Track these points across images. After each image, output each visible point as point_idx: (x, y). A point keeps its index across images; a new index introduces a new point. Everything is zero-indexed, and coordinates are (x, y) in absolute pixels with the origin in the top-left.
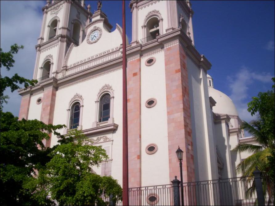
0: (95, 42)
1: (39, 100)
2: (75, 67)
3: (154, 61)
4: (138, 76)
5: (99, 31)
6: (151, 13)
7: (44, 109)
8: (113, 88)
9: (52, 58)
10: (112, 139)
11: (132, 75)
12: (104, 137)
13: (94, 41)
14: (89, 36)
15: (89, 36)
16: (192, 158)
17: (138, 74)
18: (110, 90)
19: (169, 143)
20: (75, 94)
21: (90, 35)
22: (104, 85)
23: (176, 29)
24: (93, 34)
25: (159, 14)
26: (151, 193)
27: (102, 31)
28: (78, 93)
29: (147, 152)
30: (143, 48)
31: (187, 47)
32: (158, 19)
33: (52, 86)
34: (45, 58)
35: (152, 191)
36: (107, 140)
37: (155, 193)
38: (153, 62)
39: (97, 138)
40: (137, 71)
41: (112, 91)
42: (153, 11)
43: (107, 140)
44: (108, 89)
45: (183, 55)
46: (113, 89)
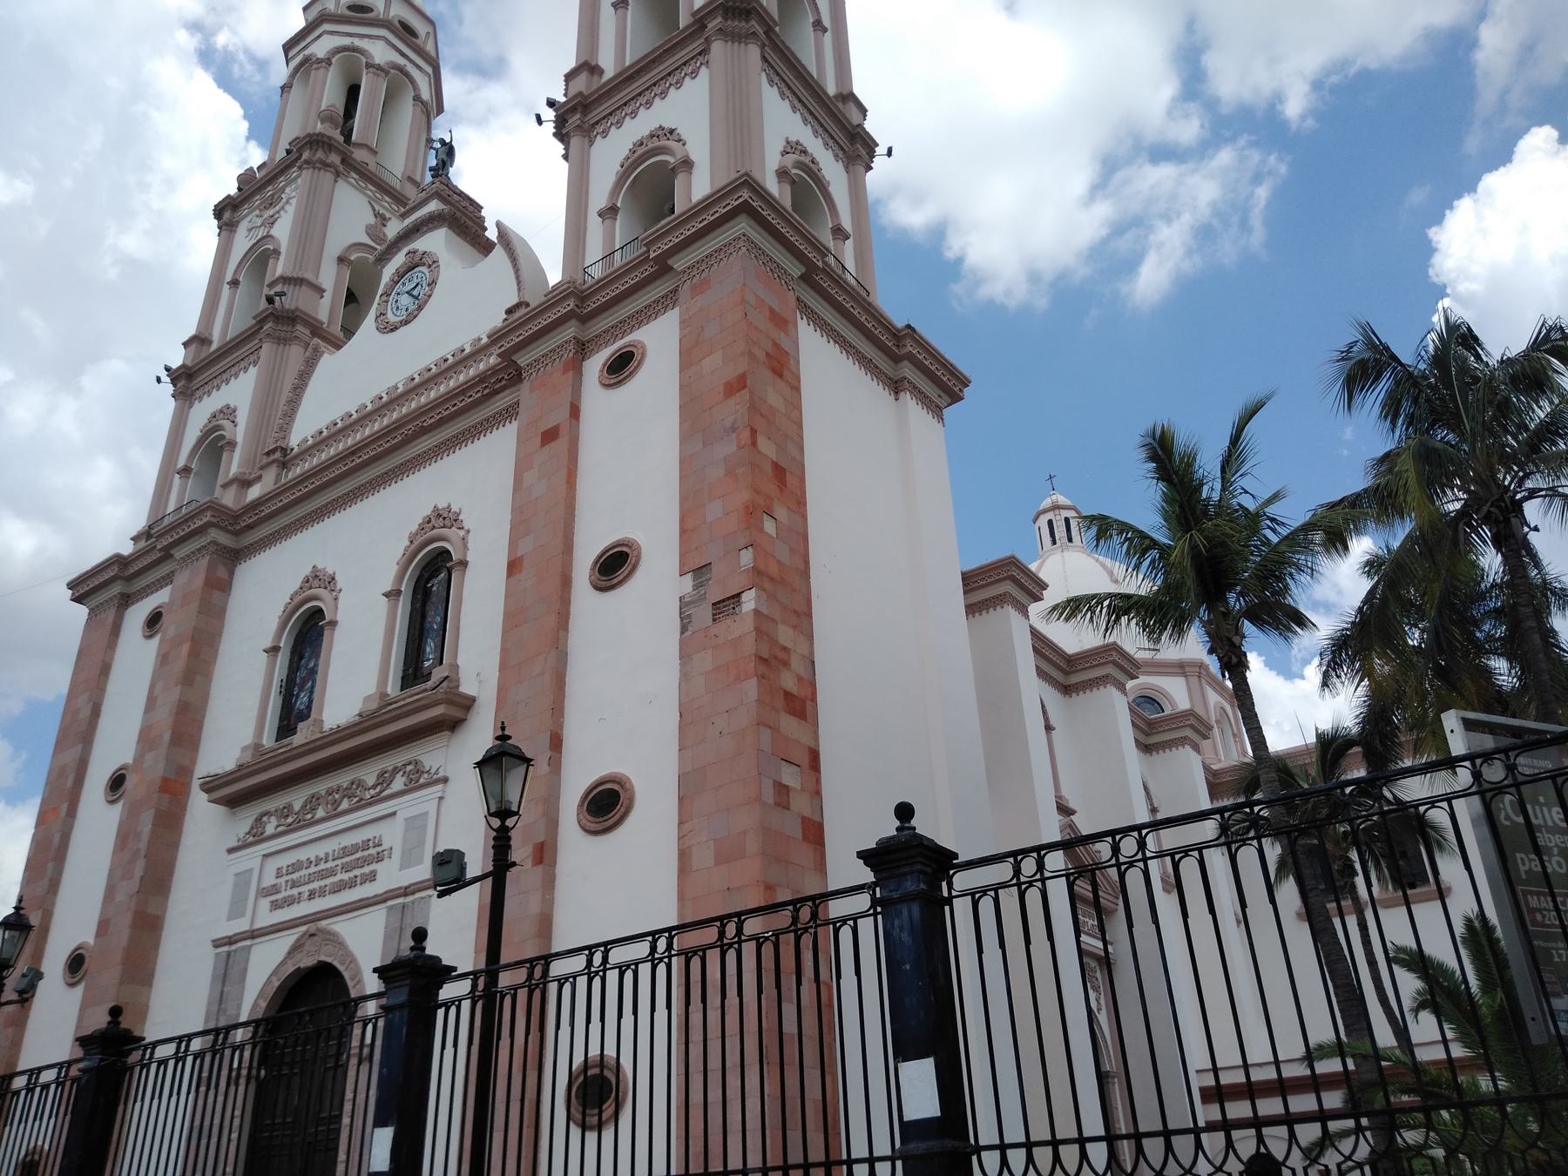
0: (406, 322)
1: (154, 621)
2: (321, 441)
3: (637, 357)
4: (561, 444)
5: (430, 266)
6: (642, 144)
7: (163, 659)
8: (467, 520)
9: (679, 140)
10: (441, 774)
11: (538, 440)
12: (409, 768)
13: (403, 315)
14: (384, 298)
15: (384, 298)
16: (805, 838)
17: (564, 432)
18: (453, 528)
19: (681, 759)
20: (307, 571)
21: (389, 295)
22: (427, 511)
23: (371, 10)
24: (404, 284)
25: (679, 140)
26: (594, 1051)
27: (438, 266)
28: (319, 567)
29: (594, 827)
30: (592, 305)
31: (802, 277)
32: (667, 162)
33: (1248, 627)
34: (206, 426)
35: (996, 901)
36: (422, 781)
37: (610, 1051)
38: (634, 364)
39: (379, 777)
40: (560, 416)
41: (462, 533)
42: (652, 136)
43: (422, 781)
44: (444, 527)
45: (772, 310)
46: (466, 525)
